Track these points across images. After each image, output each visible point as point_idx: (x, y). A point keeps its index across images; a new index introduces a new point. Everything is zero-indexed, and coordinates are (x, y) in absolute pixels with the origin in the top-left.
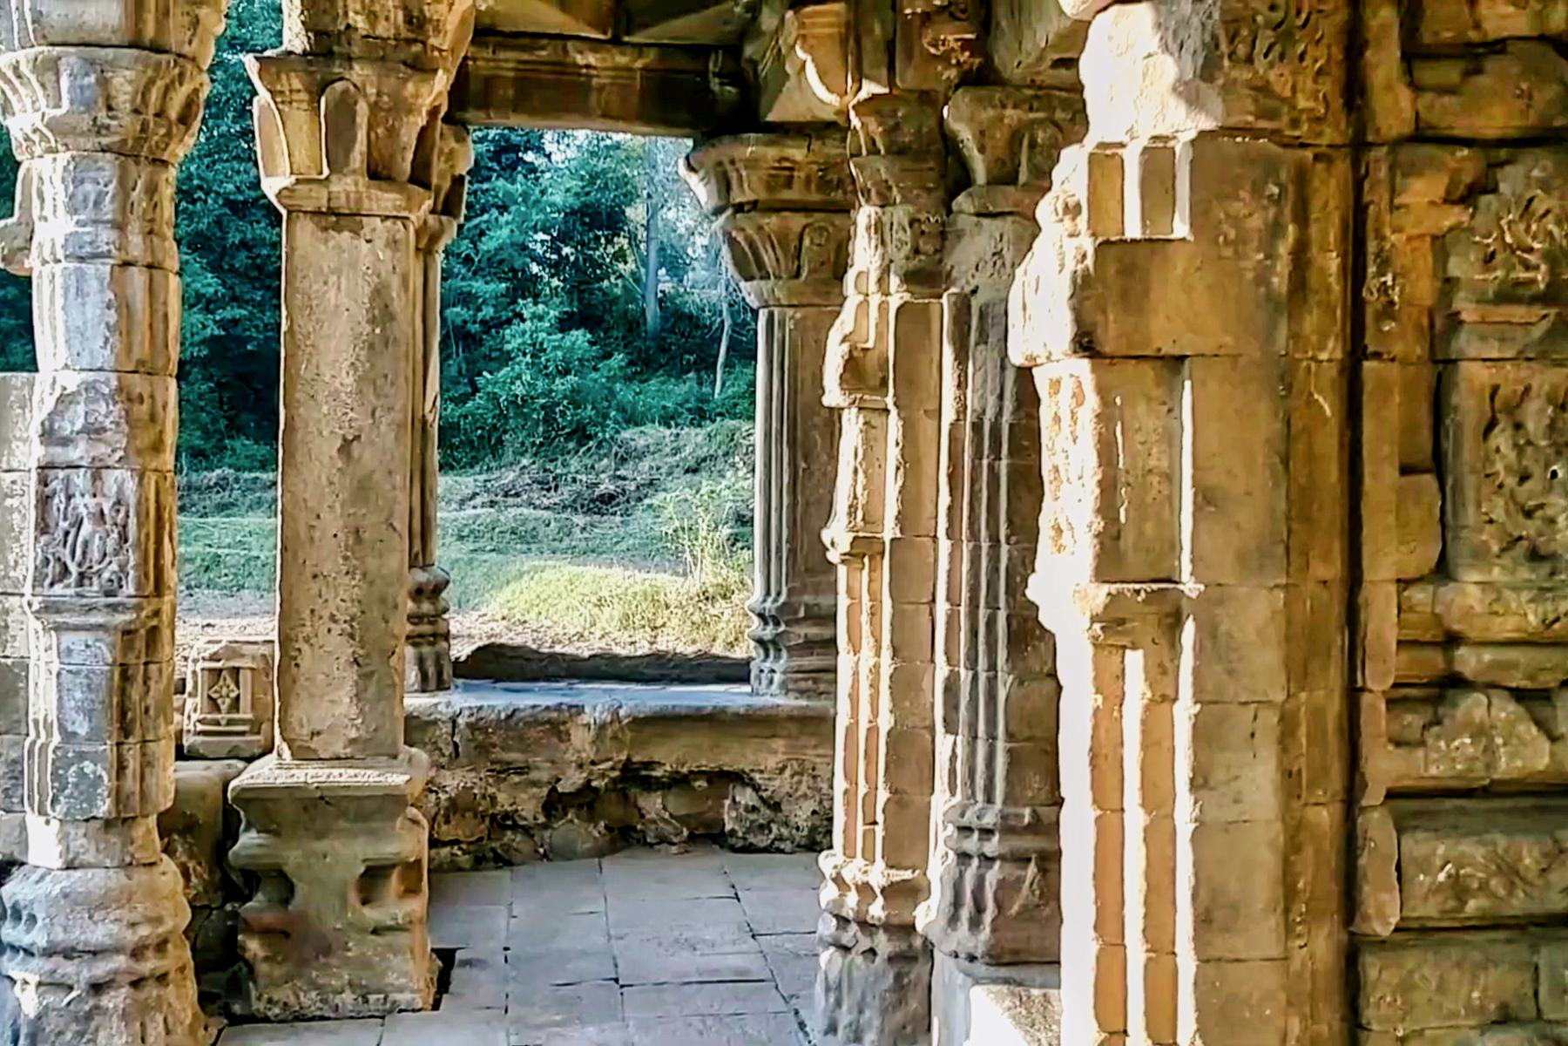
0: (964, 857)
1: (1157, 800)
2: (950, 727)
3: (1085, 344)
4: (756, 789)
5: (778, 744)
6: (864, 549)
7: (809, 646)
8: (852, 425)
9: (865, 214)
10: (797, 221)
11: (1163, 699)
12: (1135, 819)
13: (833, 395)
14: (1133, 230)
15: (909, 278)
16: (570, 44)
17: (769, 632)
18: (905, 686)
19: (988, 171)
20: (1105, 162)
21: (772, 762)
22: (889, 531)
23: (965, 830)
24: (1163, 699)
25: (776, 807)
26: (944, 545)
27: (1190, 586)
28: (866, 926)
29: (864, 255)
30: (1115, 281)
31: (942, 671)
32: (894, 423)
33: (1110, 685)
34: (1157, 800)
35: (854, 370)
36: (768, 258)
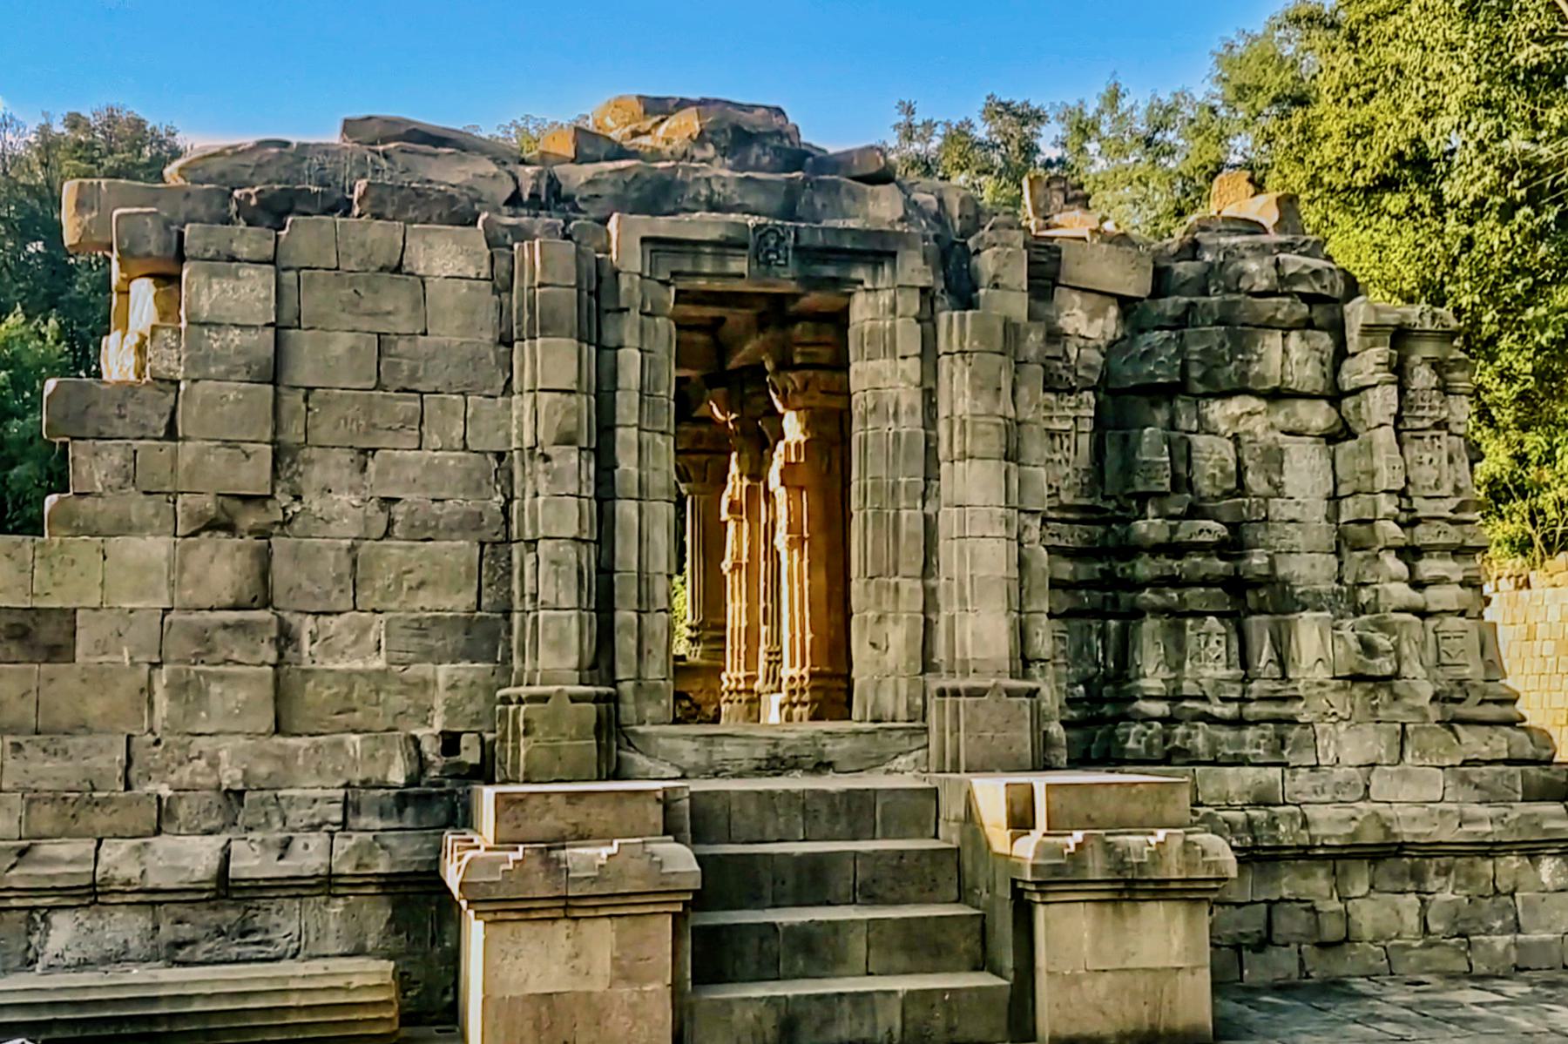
0: (770, 663)
1: (801, 582)
2: (765, 623)
3: (782, 484)
4: (690, 700)
5: (700, 680)
6: (736, 566)
7: (713, 640)
8: (731, 526)
9: (734, 456)
10: (704, 457)
11: (802, 560)
12: (796, 586)
13: (725, 516)
14: (793, 459)
15: (749, 477)
16: (1505, 755)
17: (694, 635)
18: (750, 612)
19: (1256, 818)
20: (787, 446)
21: (697, 687)
22: (745, 560)
23: (770, 654)
24: (802, 560)
25: (698, 707)
26: (763, 564)
27: (806, 535)
28: (739, 692)
29: (734, 469)
30: (788, 470)
31: (762, 605)
32: (746, 525)
33: (791, 558)
34: (801, 582)
35: (732, 507)
36: (692, 474)
